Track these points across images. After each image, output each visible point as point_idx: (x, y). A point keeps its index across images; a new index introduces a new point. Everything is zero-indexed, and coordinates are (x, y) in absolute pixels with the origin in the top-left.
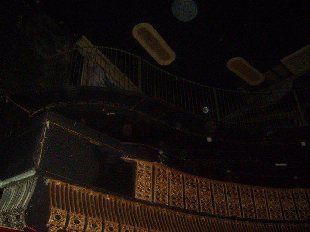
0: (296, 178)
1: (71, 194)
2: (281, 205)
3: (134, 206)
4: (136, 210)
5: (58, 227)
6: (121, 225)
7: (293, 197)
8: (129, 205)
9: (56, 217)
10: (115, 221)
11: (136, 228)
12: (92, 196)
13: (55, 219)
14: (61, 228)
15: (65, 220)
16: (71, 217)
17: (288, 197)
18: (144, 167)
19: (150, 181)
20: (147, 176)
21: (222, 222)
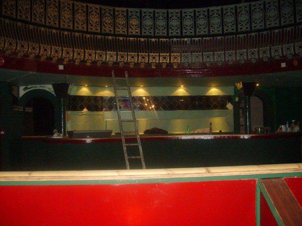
6: (18, 41)
19: (42, 8)
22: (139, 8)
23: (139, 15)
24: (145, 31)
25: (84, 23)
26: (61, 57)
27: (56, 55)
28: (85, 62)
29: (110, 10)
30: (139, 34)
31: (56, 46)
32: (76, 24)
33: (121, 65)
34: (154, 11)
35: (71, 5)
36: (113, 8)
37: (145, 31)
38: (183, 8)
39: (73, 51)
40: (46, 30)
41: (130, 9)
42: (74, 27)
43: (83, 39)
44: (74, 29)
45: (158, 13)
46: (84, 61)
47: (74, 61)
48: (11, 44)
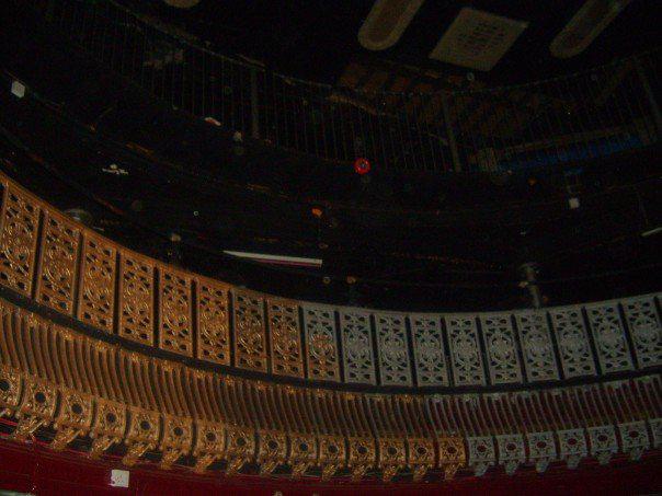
0: (175, 238)
1: (343, 406)
2: (231, 328)
3: (159, 368)
4: (317, 403)
5: (179, 450)
7: (338, 324)
8: (210, 381)
9: (175, 431)
10: (217, 421)
11: (260, 431)
12: (408, 405)
13: (418, 454)
14: (370, 466)
15: (124, 422)
16: (200, 430)
17: (289, 319)
18: (390, 322)
19: (148, 300)
20: (361, 337)
21: (218, 380)
22: (473, 310)
23: (617, 316)
24: (646, 355)
25: (623, 350)
26: (558, 457)
27: (604, 446)
28: (350, 471)
29: (503, 321)
30: (630, 366)
31: (478, 435)
32: (492, 369)
33: (511, 469)
34: (655, 298)
35: (616, 310)
36: (509, 316)
37: (646, 355)
38: (411, 309)
39: (436, 446)
40: (415, 401)
41: (590, 307)
42: (451, 378)
43: (454, 407)
44: (488, 381)
45: (418, 323)
46: (346, 470)
47: (502, 468)
48: (362, 451)
